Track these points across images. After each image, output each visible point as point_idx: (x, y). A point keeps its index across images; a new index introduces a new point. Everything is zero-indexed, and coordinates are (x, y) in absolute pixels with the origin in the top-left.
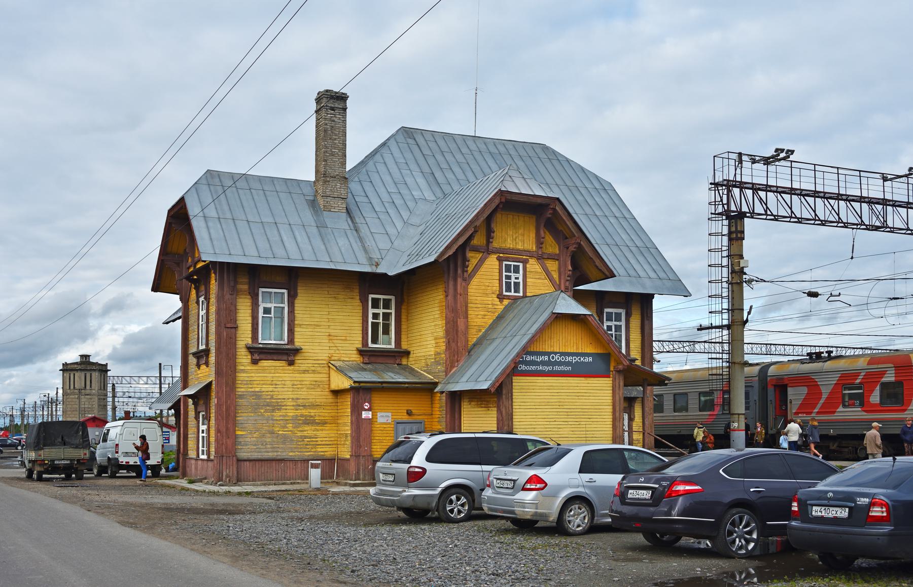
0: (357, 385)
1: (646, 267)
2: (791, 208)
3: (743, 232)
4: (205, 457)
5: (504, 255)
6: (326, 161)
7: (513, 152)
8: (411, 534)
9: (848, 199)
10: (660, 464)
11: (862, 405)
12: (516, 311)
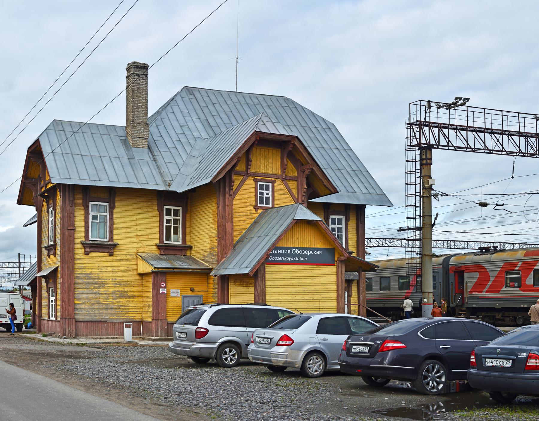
0: (156, 270)
1: (360, 185)
2: (467, 141)
3: (431, 159)
4: (54, 319)
5: (259, 177)
6: (133, 112)
7: (263, 103)
8: (199, 375)
9: (510, 134)
10: (374, 328)
11: (520, 286)
12: (267, 218)
